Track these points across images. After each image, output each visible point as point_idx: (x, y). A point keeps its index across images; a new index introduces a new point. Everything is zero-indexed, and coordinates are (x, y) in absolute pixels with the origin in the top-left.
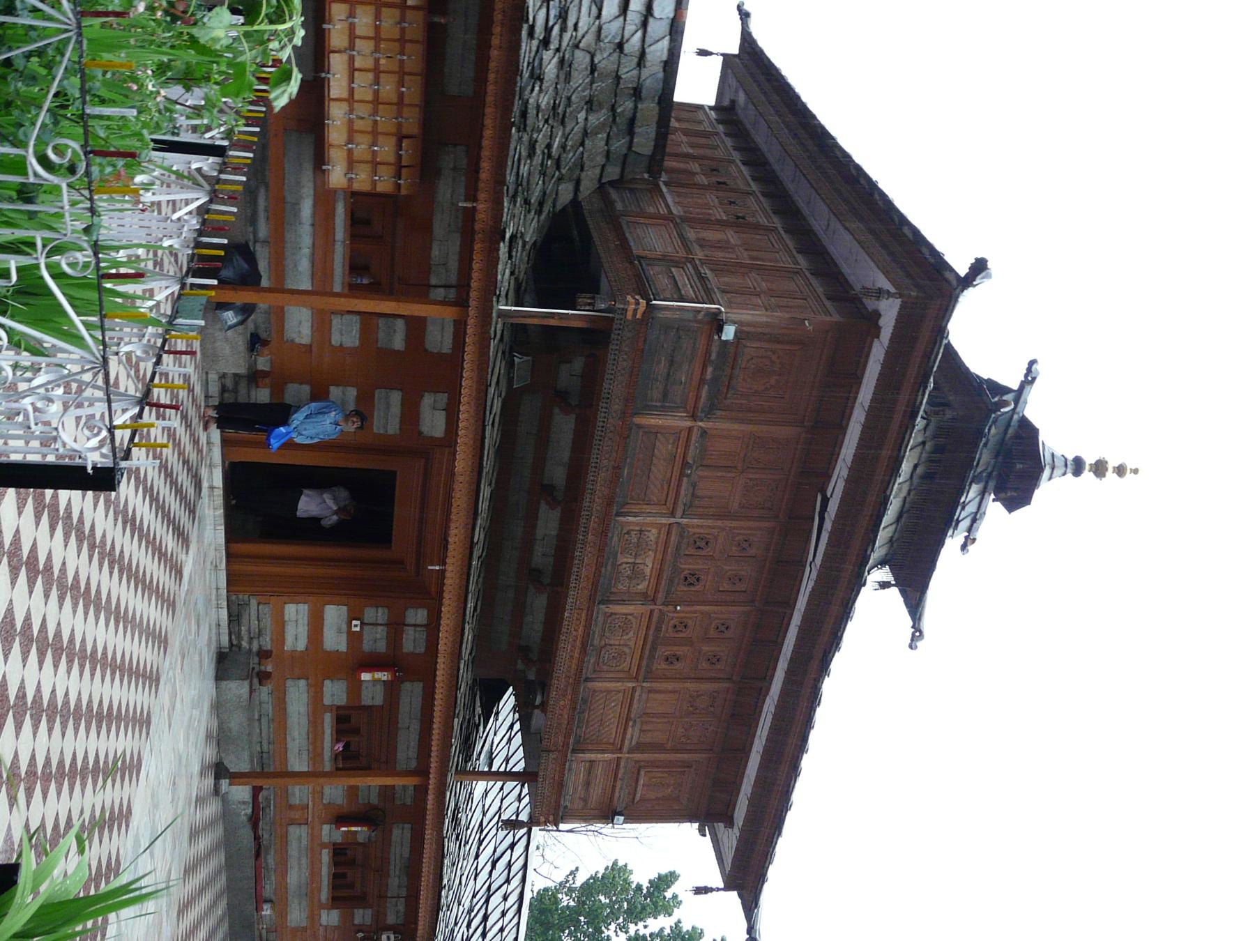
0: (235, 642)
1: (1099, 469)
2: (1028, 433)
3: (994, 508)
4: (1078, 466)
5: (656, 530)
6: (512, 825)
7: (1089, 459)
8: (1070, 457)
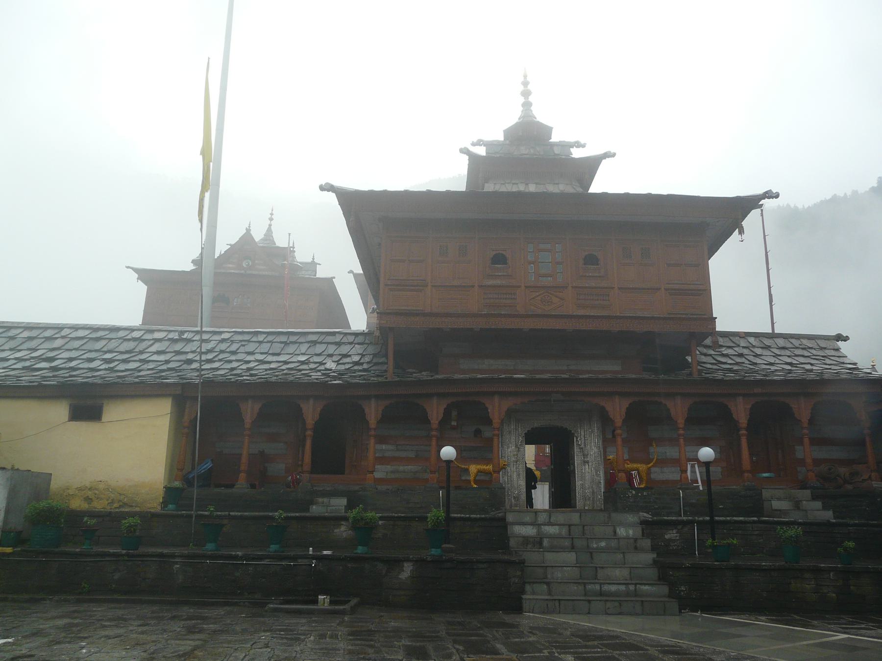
7: (522, 100)
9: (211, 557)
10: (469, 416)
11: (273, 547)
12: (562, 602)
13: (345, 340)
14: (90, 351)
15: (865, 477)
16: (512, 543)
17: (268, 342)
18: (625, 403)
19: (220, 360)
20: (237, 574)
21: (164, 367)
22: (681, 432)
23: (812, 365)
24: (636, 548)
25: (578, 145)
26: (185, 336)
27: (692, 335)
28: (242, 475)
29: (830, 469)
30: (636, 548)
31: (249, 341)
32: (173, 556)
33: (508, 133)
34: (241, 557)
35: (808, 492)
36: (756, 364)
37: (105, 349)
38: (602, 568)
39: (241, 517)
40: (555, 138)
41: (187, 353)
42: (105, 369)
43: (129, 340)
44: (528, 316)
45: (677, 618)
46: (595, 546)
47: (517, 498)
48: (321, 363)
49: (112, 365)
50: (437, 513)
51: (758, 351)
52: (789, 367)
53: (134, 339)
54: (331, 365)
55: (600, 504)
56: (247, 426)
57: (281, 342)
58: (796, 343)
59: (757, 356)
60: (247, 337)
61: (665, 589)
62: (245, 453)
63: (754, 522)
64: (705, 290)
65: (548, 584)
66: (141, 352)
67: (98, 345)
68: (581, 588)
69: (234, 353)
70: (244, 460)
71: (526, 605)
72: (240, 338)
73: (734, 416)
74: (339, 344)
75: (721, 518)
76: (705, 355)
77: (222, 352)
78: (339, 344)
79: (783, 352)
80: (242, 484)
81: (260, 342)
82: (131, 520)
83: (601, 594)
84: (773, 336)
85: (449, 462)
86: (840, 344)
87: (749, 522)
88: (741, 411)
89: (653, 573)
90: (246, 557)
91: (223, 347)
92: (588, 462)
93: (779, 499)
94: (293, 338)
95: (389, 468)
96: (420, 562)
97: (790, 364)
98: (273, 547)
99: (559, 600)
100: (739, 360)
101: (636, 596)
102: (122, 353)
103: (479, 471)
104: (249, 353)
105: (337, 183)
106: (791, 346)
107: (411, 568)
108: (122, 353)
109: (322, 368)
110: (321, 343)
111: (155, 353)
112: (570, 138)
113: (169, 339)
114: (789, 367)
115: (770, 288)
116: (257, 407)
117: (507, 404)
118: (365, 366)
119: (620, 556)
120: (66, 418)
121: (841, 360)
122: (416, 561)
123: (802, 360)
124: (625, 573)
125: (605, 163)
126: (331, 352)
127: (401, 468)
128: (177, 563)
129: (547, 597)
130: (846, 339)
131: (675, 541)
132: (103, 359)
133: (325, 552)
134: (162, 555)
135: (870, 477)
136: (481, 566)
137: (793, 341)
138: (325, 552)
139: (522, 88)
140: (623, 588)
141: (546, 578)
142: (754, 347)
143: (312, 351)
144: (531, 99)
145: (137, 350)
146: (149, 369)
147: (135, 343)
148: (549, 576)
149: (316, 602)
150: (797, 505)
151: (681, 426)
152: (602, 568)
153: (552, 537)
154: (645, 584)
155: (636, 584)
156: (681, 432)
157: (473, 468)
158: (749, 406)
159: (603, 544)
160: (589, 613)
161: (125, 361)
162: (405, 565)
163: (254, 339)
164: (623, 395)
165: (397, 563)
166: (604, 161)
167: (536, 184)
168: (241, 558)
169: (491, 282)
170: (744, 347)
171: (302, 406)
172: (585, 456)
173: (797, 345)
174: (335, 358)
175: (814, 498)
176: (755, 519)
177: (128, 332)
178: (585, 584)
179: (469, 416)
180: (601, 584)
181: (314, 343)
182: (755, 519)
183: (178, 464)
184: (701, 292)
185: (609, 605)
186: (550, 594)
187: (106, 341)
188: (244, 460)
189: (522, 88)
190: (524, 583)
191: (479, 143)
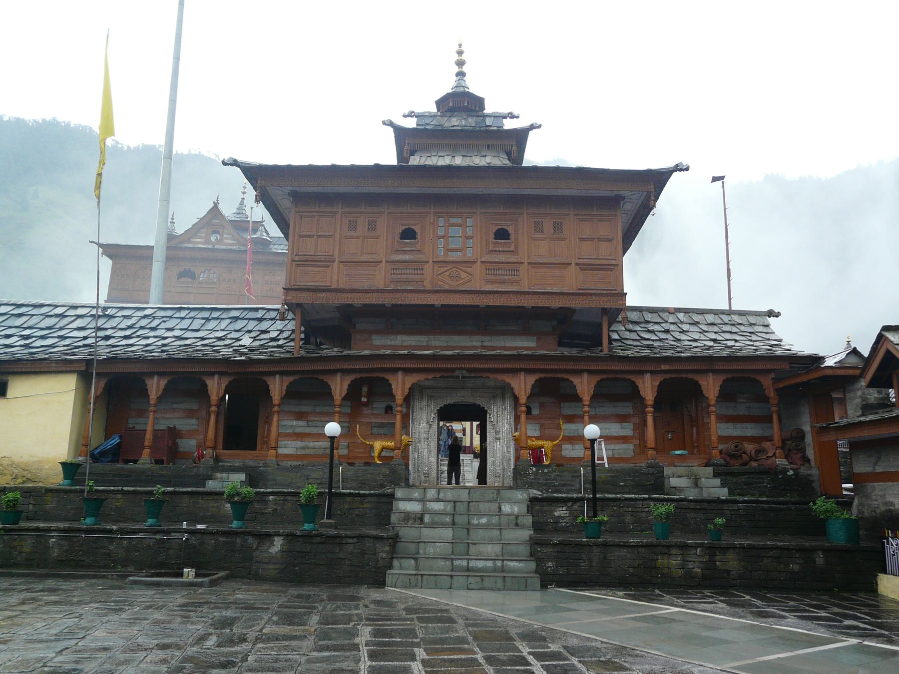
1: (460, 63)
4: (461, 74)
7: (456, 69)
8: (455, 78)
9: (86, 531)
10: (369, 392)
12: (425, 577)
13: (267, 316)
14: (10, 327)
15: (770, 454)
16: (394, 518)
17: (190, 318)
18: (531, 380)
19: (138, 336)
20: (111, 548)
21: (80, 344)
22: (586, 409)
23: (736, 341)
24: (517, 525)
25: (512, 116)
26: (108, 312)
27: (605, 311)
28: (146, 451)
29: (736, 446)
30: (517, 525)
31: (171, 317)
32: (49, 530)
33: (440, 103)
34: (116, 531)
35: (710, 470)
36: (679, 340)
37: (25, 326)
38: (475, 544)
39: (134, 492)
40: (490, 108)
41: (107, 329)
42: (21, 346)
43: (52, 316)
44: (436, 292)
45: (538, 594)
46: (476, 522)
47: (427, 475)
48: (238, 340)
49: (27, 342)
50: (311, 489)
51: (685, 327)
52: (711, 343)
53: (57, 316)
54: (246, 341)
55: (509, 482)
56: (152, 402)
57: (203, 319)
58: (726, 318)
59: (683, 332)
60: (169, 313)
61: (532, 565)
62: (149, 429)
63: (645, 499)
64: (617, 265)
65: (416, 559)
66: (61, 329)
67: (19, 322)
68: (448, 563)
69: (154, 329)
70: (149, 436)
71: (389, 579)
72: (162, 313)
74: (260, 320)
75: (612, 496)
76: (630, 331)
77: (142, 328)
78: (260, 320)
79: (711, 328)
80: (145, 460)
81: (183, 318)
82: (11, 496)
83: (468, 569)
84: (730, 312)
86: (771, 320)
87: (640, 500)
88: (648, 388)
89: (525, 550)
90: (121, 531)
91: (144, 322)
92: (499, 439)
93: (680, 476)
94: (215, 314)
95: (299, 444)
96: (290, 537)
97: (715, 340)
98: (150, 521)
99: (422, 575)
100: (663, 336)
101: (503, 571)
102: (42, 329)
103: (383, 448)
104: (168, 329)
105: (240, 159)
106: (721, 322)
107: (281, 542)
108: (42, 329)
109: (237, 344)
110: (242, 319)
111: (75, 329)
112: (504, 110)
113: (92, 316)
114: (711, 343)
115: (728, 262)
116: (163, 383)
117: (411, 380)
118: (281, 342)
119: (496, 533)
121: (767, 336)
122: (287, 535)
123: (728, 336)
124: (497, 549)
125: (532, 133)
126: (249, 328)
127: (311, 444)
128: (53, 537)
129: (414, 572)
130: (777, 315)
131: (564, 518)
132: (21, 336)
133: (199, 527)
134: (38, 529)
135: (774, 454)
136: (351, 541)
137: (723, 316)
138: (199, 527)
140: (489, 564)
141: (418, 553)
142: (682, 323)
143: (231, 327)
144: (465, 69)
145: (57, 326)
146: (64, 346)
147: (57, 320)
148: (421, 552)
149: (181, 575)
150: (696, 484)
152: (475, 544)
153: (434, 513)
154: (512, 560)
155: (503, 560)
156: (586, 409)
157: (378, 445)
158: (657, 383)
159: (484, 520)
160: (451, 588)
161: (43, 337)
162: (276, 539)
163: (177, 315)
164: (344, 372)
165: (265, 537)
166: (531, 132)
167: (464, 156)
168: (115, 532)
169: (400, 257)
170: (671, 323)
171: (701, 382)
172: (497, 432)
173: (726, 321)
174: (253, 334)
175: (716, 475)
176: (646, 496)
177: (51, 308)
178: (452, 560)
179: (369, 392)
180: (468, 560)
181: (236, 319)
182: (646, 496)
183: (81, 441)
184: (615, 269)
185: (471, 580)
186: (417, 569)
187: (28, 317)
188: (149, 436)
189: (456, 57)
190: (392, 558)
191: (411, 115)
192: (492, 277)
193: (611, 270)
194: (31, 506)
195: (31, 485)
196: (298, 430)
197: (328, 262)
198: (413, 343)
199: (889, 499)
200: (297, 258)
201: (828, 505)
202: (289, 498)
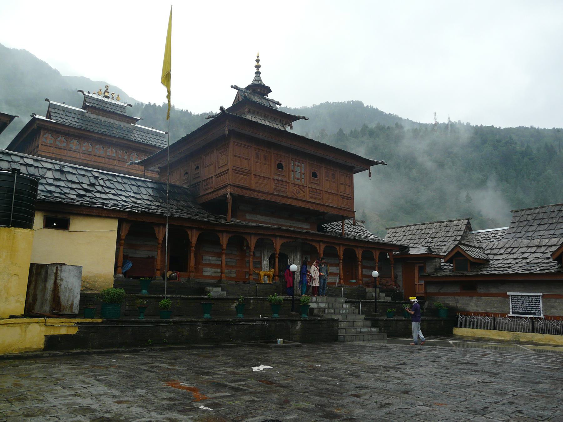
0: (23, 333)
1: (258, 67)
2: (249, 87)
3: (270, 96)
4: (258, 73)
5: (297, 182)
6: (354, 224)
7: (255, 70)
8: (255, 75)
11: (207, 315)
20: (230, 330)
39: (187, 299)
73: (221, 242)
85: (375, 278)
90: (234, 321)
95: (213, 270)
112: (276, 100)
120: (42, 226)
128: (199, 326)
134: (191, 322)
138: (265, 318)
139: (255, 63)
144: (260, 70)
151: (225, 248)
165: (294, 322)
168: (231, 322)
169: (277, 178)
192: (313, 196)
193: (227, 173)
194: (127, 307)
195: (89, 292)
196: (213, 262)
197: (248, 173)
198: (263, 220)
199: (446, 302)
200: (234, 168)
201: (473, 304)
202: (259, 301)
